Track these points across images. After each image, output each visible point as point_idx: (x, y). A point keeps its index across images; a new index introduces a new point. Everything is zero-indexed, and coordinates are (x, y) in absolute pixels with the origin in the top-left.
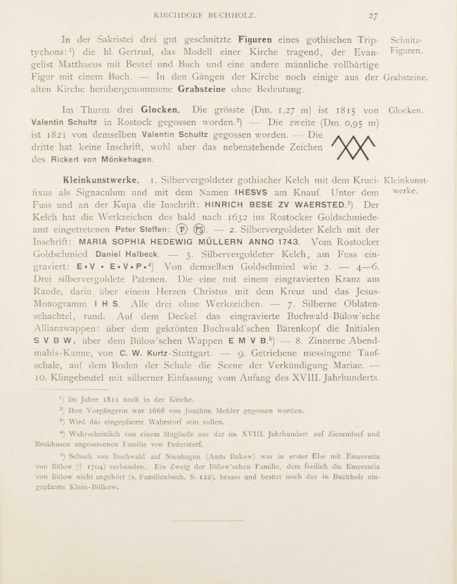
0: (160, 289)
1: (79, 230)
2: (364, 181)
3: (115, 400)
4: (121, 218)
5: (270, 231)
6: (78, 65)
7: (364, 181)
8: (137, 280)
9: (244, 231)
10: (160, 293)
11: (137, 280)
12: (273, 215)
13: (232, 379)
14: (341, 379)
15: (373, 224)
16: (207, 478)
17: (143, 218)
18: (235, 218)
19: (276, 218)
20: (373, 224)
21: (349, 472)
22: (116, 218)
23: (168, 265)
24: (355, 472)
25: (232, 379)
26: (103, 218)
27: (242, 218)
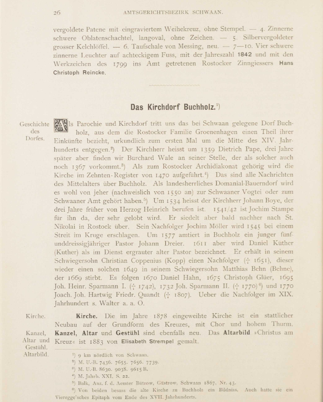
0: (91, 293)
1: (230, 150)
2: (92, 236)
3: (203, 244)
4: (70, 65)
5: (56, 31)
6: (284, 243)
7: (92, 236)
8: (119, 244)
9: (223, 30)
10: (91, 296)
11: (119, 244)
12: (90, 225)
13: (120, 398)
14: (238, 333)
15: (291, 162)
16: (125, 377)
17: (84, 65)
18: (259, 261)
19: (92, 227)
20: (291, 162)
21: (184, 394)
22: (66, 65)
23: (245, 191)
24: (189, 394)
25: (120, 398)
26: (57, 65)
27: (170, 287)
